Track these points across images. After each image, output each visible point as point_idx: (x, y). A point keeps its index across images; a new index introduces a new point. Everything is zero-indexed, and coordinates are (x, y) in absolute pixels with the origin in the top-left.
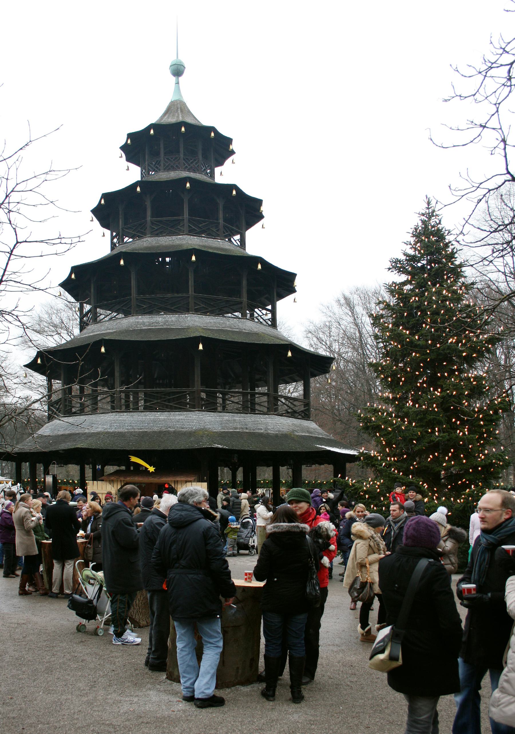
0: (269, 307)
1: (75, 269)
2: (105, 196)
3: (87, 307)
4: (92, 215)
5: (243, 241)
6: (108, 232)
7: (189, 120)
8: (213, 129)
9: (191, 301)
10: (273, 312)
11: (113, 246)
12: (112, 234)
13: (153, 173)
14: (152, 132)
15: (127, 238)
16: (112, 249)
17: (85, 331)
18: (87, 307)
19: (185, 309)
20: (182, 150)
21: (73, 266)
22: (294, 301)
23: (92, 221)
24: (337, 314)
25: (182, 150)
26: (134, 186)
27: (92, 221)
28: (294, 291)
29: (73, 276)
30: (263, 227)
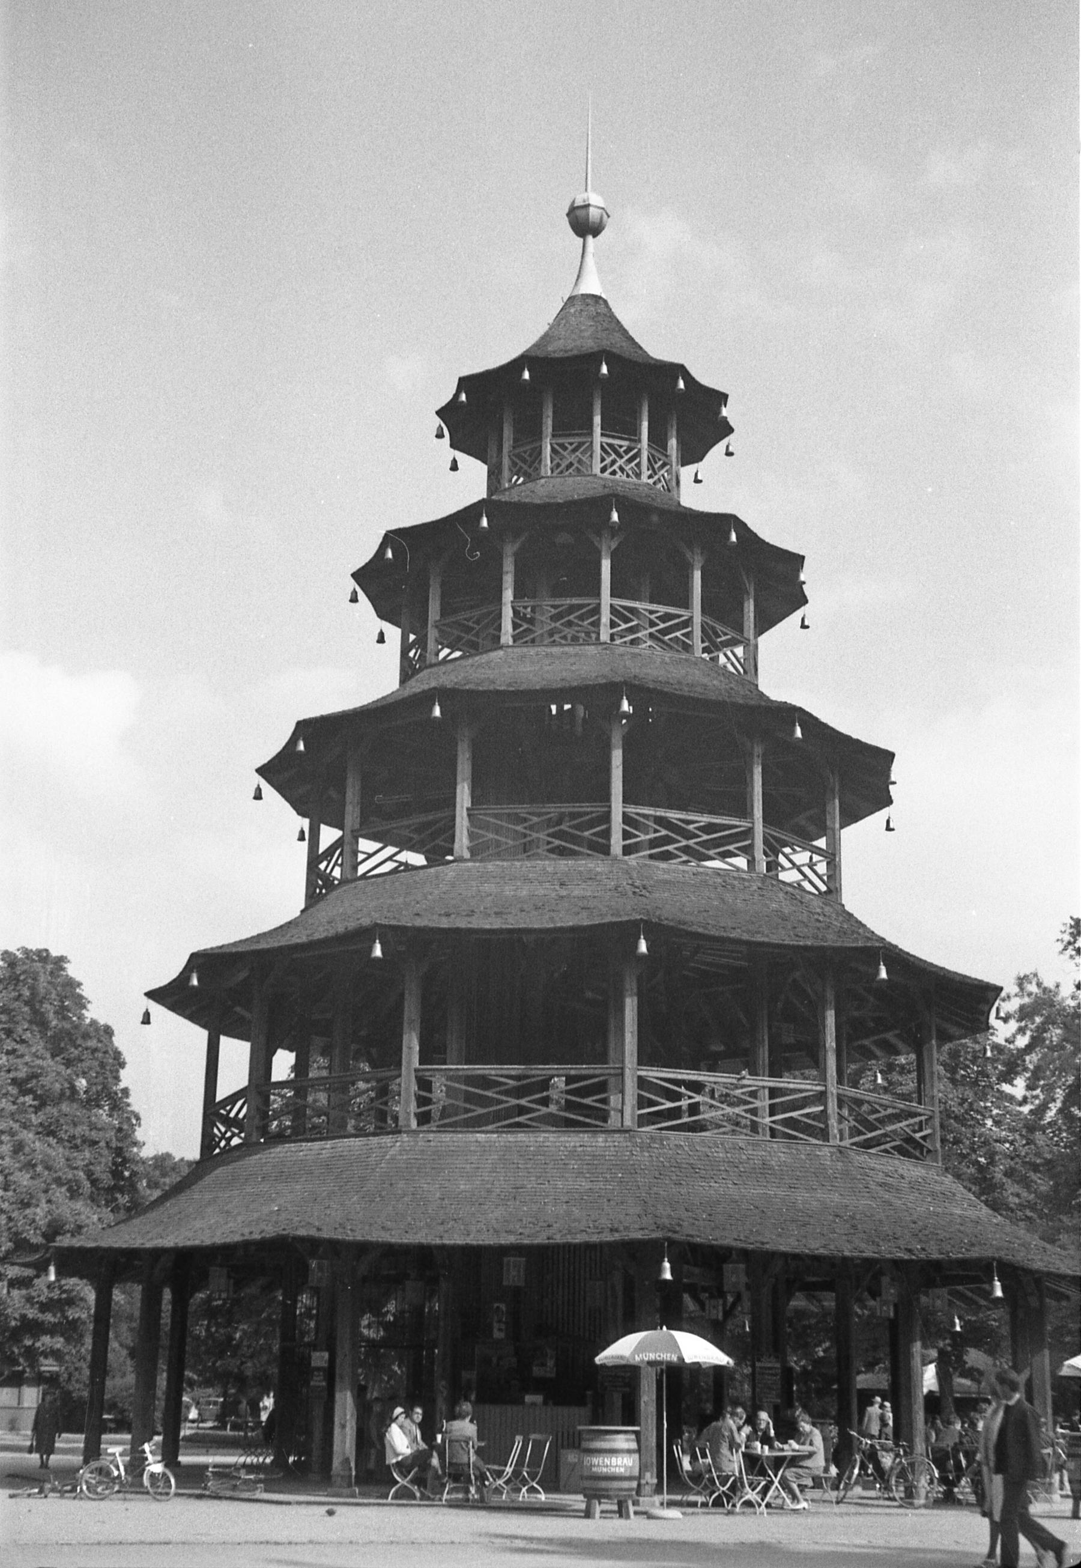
0: (821, 843)
1: (305, 728)
2: (465, 383)
3: (329, 835)
4: (352, 584)
5: (751, 664)
6: (393, 633)
7: (615, 344)
8: (680, 370)
10: (832, 857)
11: (408, 671)
12: (404, 638)
13: (521, 480)
15: (446, 651)
16: (405, 678)
17: (412, 682)
18: (329, 835)
21: (301, 718)
22: (888, 829)
23: (354, 599)
24: (990, 1037)
26: (470, 513)
27: (258, 796)
28: (889, 801)
29: (463, 397)
30: (804, 626)
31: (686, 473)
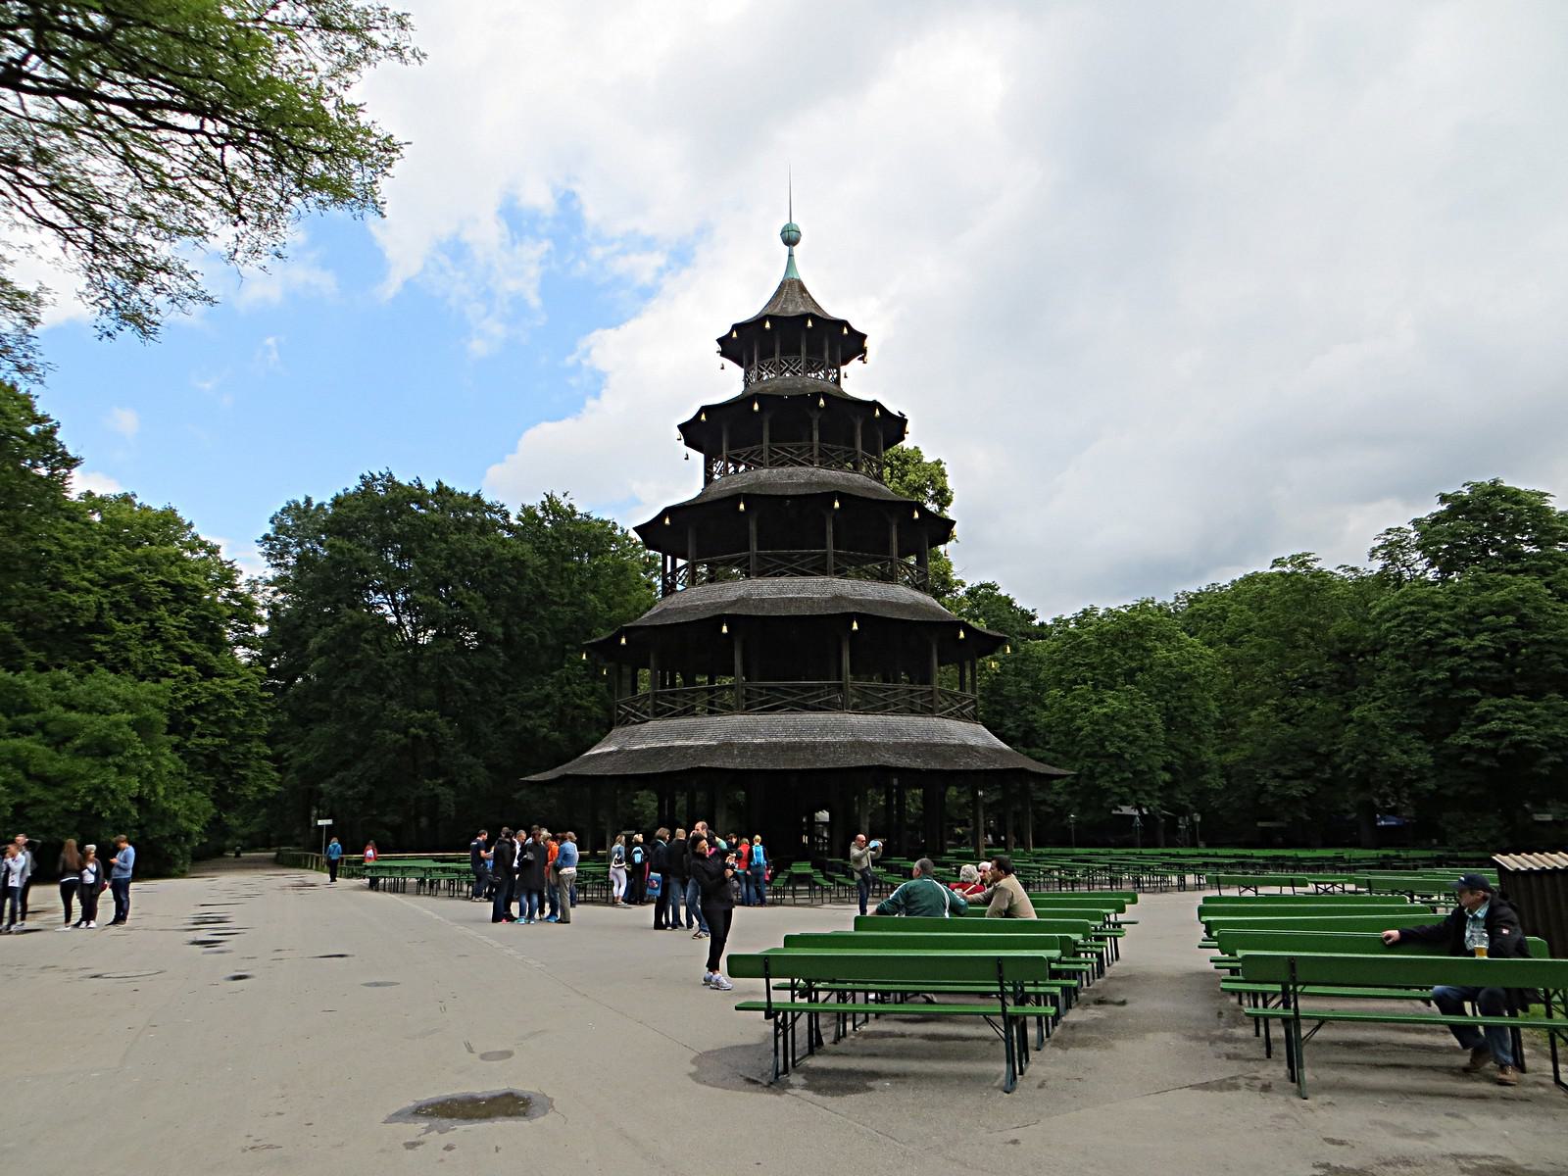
7: (814, 311)
9: (831, 559)
14: (768, 325)
19: (820, 569)
20: (803, 349)
25: (803, 349)
31: (843, 369)
